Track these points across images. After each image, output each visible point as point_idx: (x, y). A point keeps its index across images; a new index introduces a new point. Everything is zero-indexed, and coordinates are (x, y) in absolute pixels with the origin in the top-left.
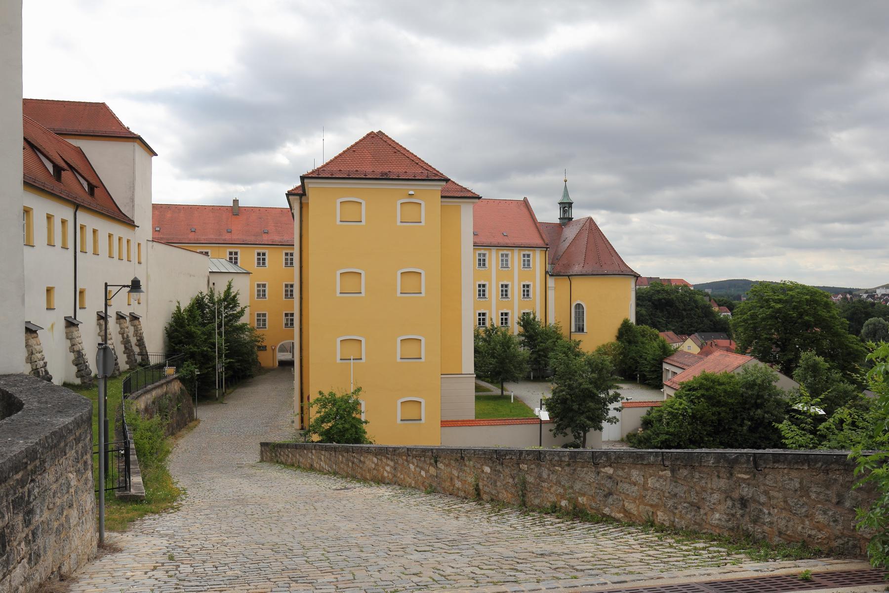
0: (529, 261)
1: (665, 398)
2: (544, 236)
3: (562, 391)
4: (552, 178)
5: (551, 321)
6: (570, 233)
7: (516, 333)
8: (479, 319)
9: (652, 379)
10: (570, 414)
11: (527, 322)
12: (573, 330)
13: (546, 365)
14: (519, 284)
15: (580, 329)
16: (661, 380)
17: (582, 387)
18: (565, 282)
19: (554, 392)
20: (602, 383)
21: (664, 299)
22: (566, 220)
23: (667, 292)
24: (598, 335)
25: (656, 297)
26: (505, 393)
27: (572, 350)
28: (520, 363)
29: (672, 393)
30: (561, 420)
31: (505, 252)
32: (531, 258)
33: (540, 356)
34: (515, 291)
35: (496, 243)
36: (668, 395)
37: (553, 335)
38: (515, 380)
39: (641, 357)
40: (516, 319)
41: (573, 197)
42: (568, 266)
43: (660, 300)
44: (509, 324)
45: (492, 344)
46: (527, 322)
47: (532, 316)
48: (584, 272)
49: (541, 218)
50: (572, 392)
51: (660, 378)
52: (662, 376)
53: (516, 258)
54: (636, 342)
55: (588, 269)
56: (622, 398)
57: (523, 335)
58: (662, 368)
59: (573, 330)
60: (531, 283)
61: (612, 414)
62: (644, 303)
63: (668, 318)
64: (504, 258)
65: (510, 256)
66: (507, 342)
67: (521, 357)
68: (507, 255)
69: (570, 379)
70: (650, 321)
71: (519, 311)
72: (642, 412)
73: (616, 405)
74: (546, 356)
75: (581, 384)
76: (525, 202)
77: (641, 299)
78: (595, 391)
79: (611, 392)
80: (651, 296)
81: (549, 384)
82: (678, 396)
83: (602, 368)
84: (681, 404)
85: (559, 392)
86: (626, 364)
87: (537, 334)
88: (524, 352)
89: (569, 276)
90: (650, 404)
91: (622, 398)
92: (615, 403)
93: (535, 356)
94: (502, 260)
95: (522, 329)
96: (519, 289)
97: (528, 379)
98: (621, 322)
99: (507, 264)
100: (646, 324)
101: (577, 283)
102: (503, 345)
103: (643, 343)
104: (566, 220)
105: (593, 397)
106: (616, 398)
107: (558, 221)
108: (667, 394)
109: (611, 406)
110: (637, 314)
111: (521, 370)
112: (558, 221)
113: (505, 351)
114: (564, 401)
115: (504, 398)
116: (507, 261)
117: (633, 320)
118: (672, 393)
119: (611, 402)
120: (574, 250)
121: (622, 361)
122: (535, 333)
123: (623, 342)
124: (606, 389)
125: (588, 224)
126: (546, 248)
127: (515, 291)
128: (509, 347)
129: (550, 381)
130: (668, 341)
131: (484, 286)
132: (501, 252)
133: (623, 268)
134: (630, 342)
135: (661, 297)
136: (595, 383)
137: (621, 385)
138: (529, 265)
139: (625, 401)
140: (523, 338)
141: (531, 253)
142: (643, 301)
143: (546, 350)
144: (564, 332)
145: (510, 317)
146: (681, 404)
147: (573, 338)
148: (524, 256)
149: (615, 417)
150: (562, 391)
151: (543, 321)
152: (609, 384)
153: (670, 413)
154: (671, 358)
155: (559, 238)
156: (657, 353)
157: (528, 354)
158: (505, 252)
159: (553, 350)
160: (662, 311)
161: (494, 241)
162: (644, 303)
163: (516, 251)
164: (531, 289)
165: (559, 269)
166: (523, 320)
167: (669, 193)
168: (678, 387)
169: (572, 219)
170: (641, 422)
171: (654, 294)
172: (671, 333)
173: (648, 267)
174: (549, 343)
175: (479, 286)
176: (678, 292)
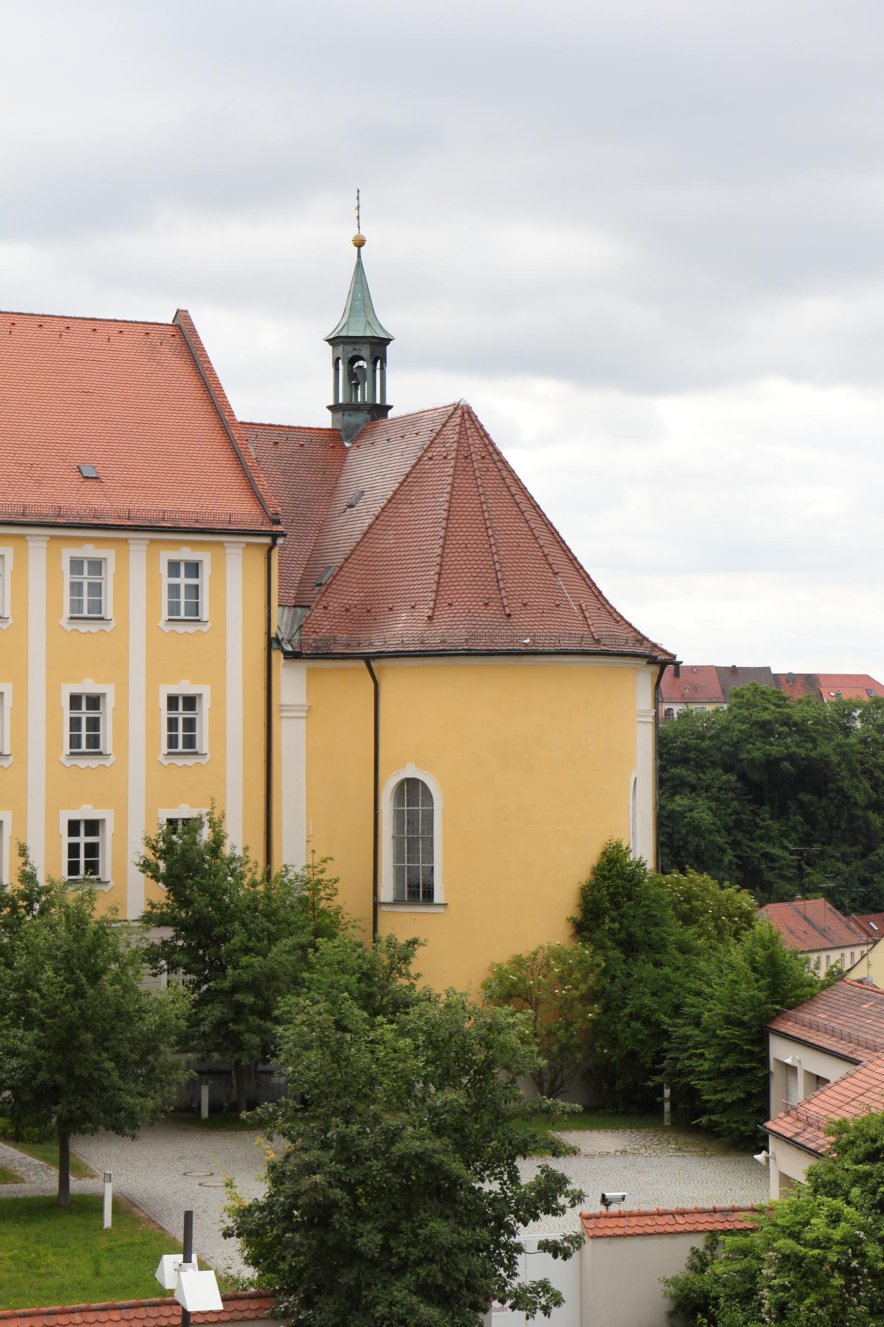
0: (194, 591)
1: (773, 1194)
2: (263, 484)
3: (310, 1169)
4: (310, 241)
5: (293, 856)
6: (375, 471)
7: (134, 908)
8: (73, 849)
9: (725, 1108)
10: (347, 1278)
11: (184, 859)
12: (387, 893)
13: (268, 1049)
14: (151, 694)
15: (418, 891)
16: (764, 1113)
17: (399, 1148)
18: (349, 686)
19: (277, 1175)
20: (487, 1134)
21: (790, 758)
22: (361, 415)
23: (799, 728)
24: (493, 922)
25: (756, 751)
26: (76, 1185)
27: (378, 988)
28: (149, 1046)
29: (797, 1167)
30: (307, 1302)
31: (89, 551)
32: (205, 580)
33: (239, 1009)
34: (135, 725)
35: (47, 511)
36: (785, 1179)
37: (298, 917)
38: (123, 1124)
39: (677, 1009)
40: (138, 850)
41: (390, 319)
42: (368, 613)
43: (771, 763)
44: (106, 870)
45: (21, 960)
46: (184, 859)
47: (206, 835)
48: (434, 643)
49: (247, 406)
50: (355, 1174)
51: (758, 1104)
52: (765, 1094)
53: (137, 576)
54: (657, 947)
55: (451, 630)
56: (577, 1198)
57: (162, 921)
58: (764, 1060)
59: (387, 893)
60: (203, 690)
61: (532, 1267)
62: (707, 777)
63: (806, 840)
64: (86, 579)
65: (110, 568)
66: (86, 952)
67: (151, 1021)
68: (97, 566)
69: (347, 1114)
70: (729, 857)
71: (150, 812)
72: (671, 1258)
73: (548, 1228)
74: (265, 1013)
75: (393, 1137)
76: (183, 334)
77: (678, 759)
78: (456, 1166)
79: (528, 1170)
80: (736, 745)
81: (259, 1139)
82: (824, 1186)
83: (490, 1064)
84: (835, 1219)
85: (296, 1177)
86: (614, 1042)
87: (227, 914)
88: (163, 991)
89: (368, 659)
90: (706, 1223)
91: (577, 1198)
92: (546, 1219)
93: (215, 1012)
94: (76, 588)
95: (160, 893)
96: (151, 712)
97: (184, 1117)
98: (591, 857)
99: (96, 606)
100: (702, 866)
101: (402, 685)
102: (67, 963)
103: (684, 949)
104: (361, 415)
105: (443, 1191)
106: (548, 1196)
107: (326, 420)
108: (772, 1182)
109: (529, 1235)
110: (665, 823)
111: (153, 1079)
112: (326, 420)
113: (79, 994)
114: (320, 1215)
115: (70, 1208)
116: (96, 589)
117: (643, 849)
118: (797, 1167)
119: (529, 1214)
120: (393, 541)
121: (597, 1030)
122: (220, 908)
123: (599, 947)
124: (504, 1160)
125: (451, 435)
126: (269, 534)
127: (135, 725)
128: (95, 977)
129: (259, 1125)
130: (788, 944)
131: (94, 702)
132: (69, 553)
133: (600, 626)
134: (630, 946)
135: (775, 750)
136: (459, 1129)
137: (570, 1138)
138: (194, 609)
139: (592, 1205)
140: (167, 933)
141: (204, 557)
142: (700, 767)
143: (265, 988)
144: (349, 901)
145: (107, 840)
146: (835, 1219)
147: (384, 932)
148: (174, 568)
149: (544, 1286)
150: (310, 1169)
151: (257, 855)
152: (520, 1130)
153: (788, 1261)
154: (805, 1015)
155: (332, 493)
156: (745, 992)
157: (184, 1006)
158: (89, 551)
159: (297, 983)
160: (781, 813)
161: (40, 500)
162: (707, 777)
163: (138, 549)
164: (108, 715)
165: (326, 628)
166: (167, 853)
167: (820, 313)
168: (823, 1142)
169: (383, 410)
170: (666, 1305)
171: (746, 738)
172: (818, 907)
173: (716, 623)
174: (280, 952)
175: (75, 701)
176: (847, 731)
